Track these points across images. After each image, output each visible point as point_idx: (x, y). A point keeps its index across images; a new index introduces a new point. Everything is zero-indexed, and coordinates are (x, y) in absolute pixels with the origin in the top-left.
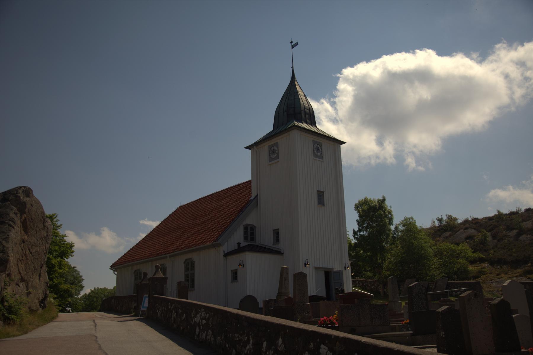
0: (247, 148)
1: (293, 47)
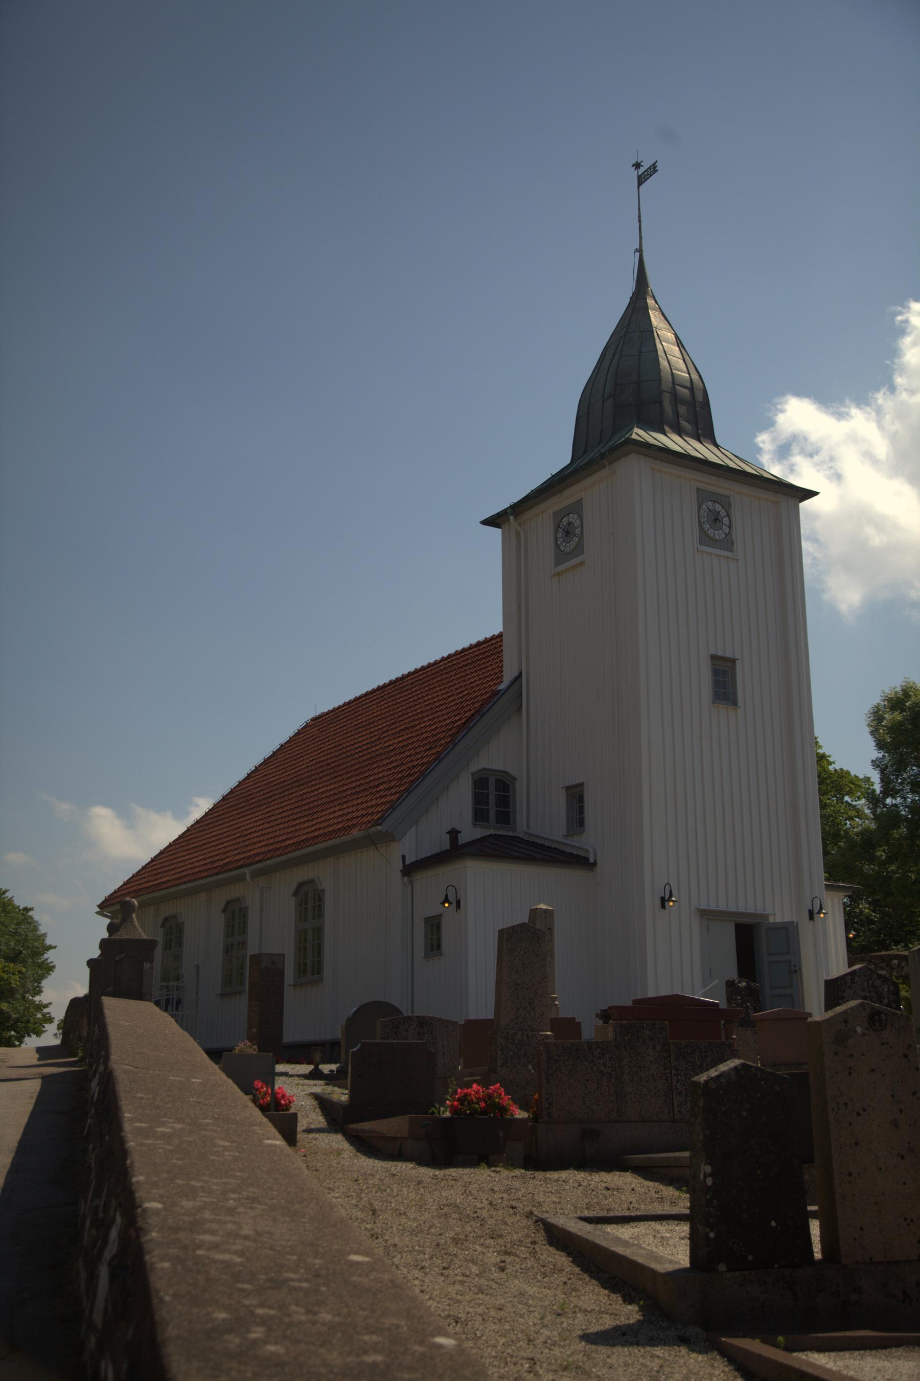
0: (486, 522)
1: (641, 180)
